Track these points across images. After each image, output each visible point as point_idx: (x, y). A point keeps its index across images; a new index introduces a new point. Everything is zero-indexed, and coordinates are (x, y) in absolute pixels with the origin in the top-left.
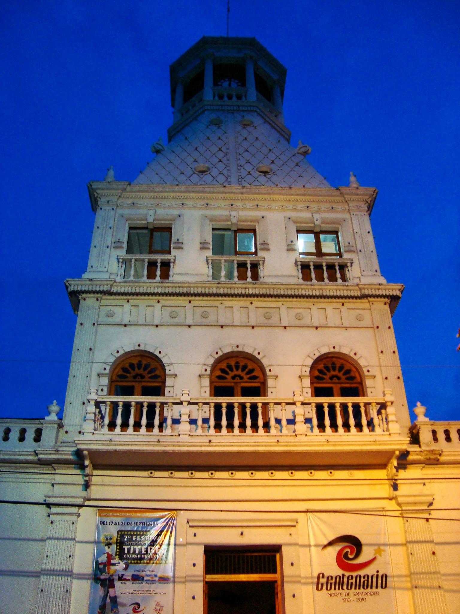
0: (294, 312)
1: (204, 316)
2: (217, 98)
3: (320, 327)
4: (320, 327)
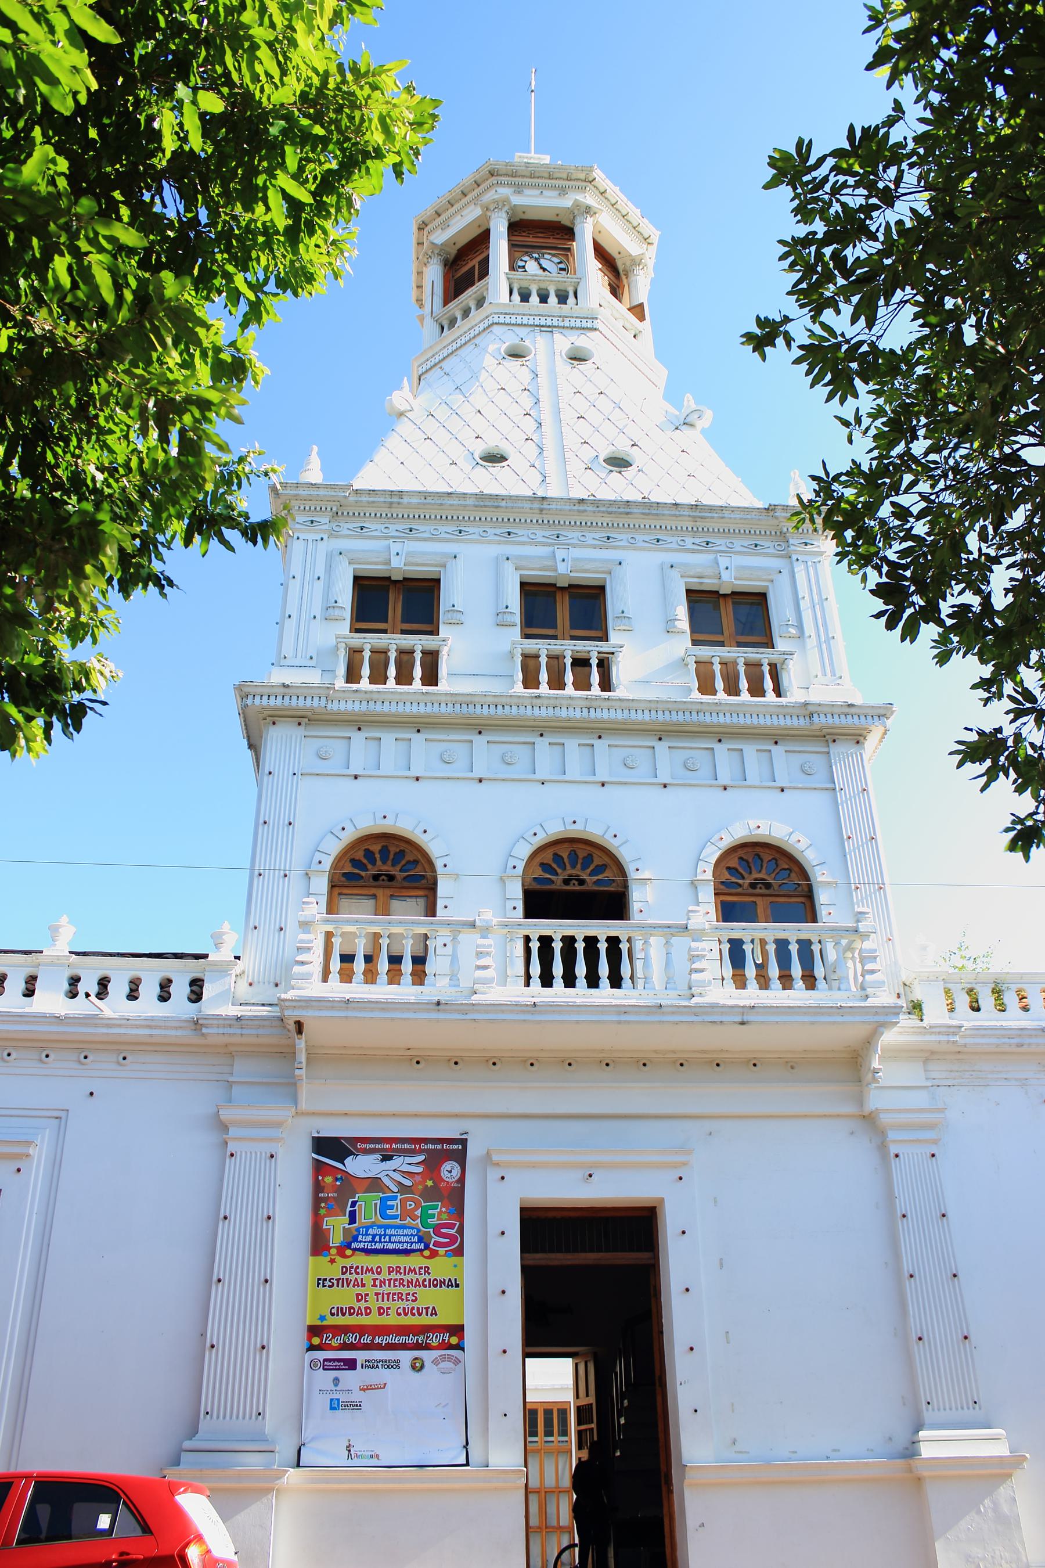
0: (680, 756)
1: (629, 762)
2: (516, 297)
3: (790, 788)
4: (790, 788)
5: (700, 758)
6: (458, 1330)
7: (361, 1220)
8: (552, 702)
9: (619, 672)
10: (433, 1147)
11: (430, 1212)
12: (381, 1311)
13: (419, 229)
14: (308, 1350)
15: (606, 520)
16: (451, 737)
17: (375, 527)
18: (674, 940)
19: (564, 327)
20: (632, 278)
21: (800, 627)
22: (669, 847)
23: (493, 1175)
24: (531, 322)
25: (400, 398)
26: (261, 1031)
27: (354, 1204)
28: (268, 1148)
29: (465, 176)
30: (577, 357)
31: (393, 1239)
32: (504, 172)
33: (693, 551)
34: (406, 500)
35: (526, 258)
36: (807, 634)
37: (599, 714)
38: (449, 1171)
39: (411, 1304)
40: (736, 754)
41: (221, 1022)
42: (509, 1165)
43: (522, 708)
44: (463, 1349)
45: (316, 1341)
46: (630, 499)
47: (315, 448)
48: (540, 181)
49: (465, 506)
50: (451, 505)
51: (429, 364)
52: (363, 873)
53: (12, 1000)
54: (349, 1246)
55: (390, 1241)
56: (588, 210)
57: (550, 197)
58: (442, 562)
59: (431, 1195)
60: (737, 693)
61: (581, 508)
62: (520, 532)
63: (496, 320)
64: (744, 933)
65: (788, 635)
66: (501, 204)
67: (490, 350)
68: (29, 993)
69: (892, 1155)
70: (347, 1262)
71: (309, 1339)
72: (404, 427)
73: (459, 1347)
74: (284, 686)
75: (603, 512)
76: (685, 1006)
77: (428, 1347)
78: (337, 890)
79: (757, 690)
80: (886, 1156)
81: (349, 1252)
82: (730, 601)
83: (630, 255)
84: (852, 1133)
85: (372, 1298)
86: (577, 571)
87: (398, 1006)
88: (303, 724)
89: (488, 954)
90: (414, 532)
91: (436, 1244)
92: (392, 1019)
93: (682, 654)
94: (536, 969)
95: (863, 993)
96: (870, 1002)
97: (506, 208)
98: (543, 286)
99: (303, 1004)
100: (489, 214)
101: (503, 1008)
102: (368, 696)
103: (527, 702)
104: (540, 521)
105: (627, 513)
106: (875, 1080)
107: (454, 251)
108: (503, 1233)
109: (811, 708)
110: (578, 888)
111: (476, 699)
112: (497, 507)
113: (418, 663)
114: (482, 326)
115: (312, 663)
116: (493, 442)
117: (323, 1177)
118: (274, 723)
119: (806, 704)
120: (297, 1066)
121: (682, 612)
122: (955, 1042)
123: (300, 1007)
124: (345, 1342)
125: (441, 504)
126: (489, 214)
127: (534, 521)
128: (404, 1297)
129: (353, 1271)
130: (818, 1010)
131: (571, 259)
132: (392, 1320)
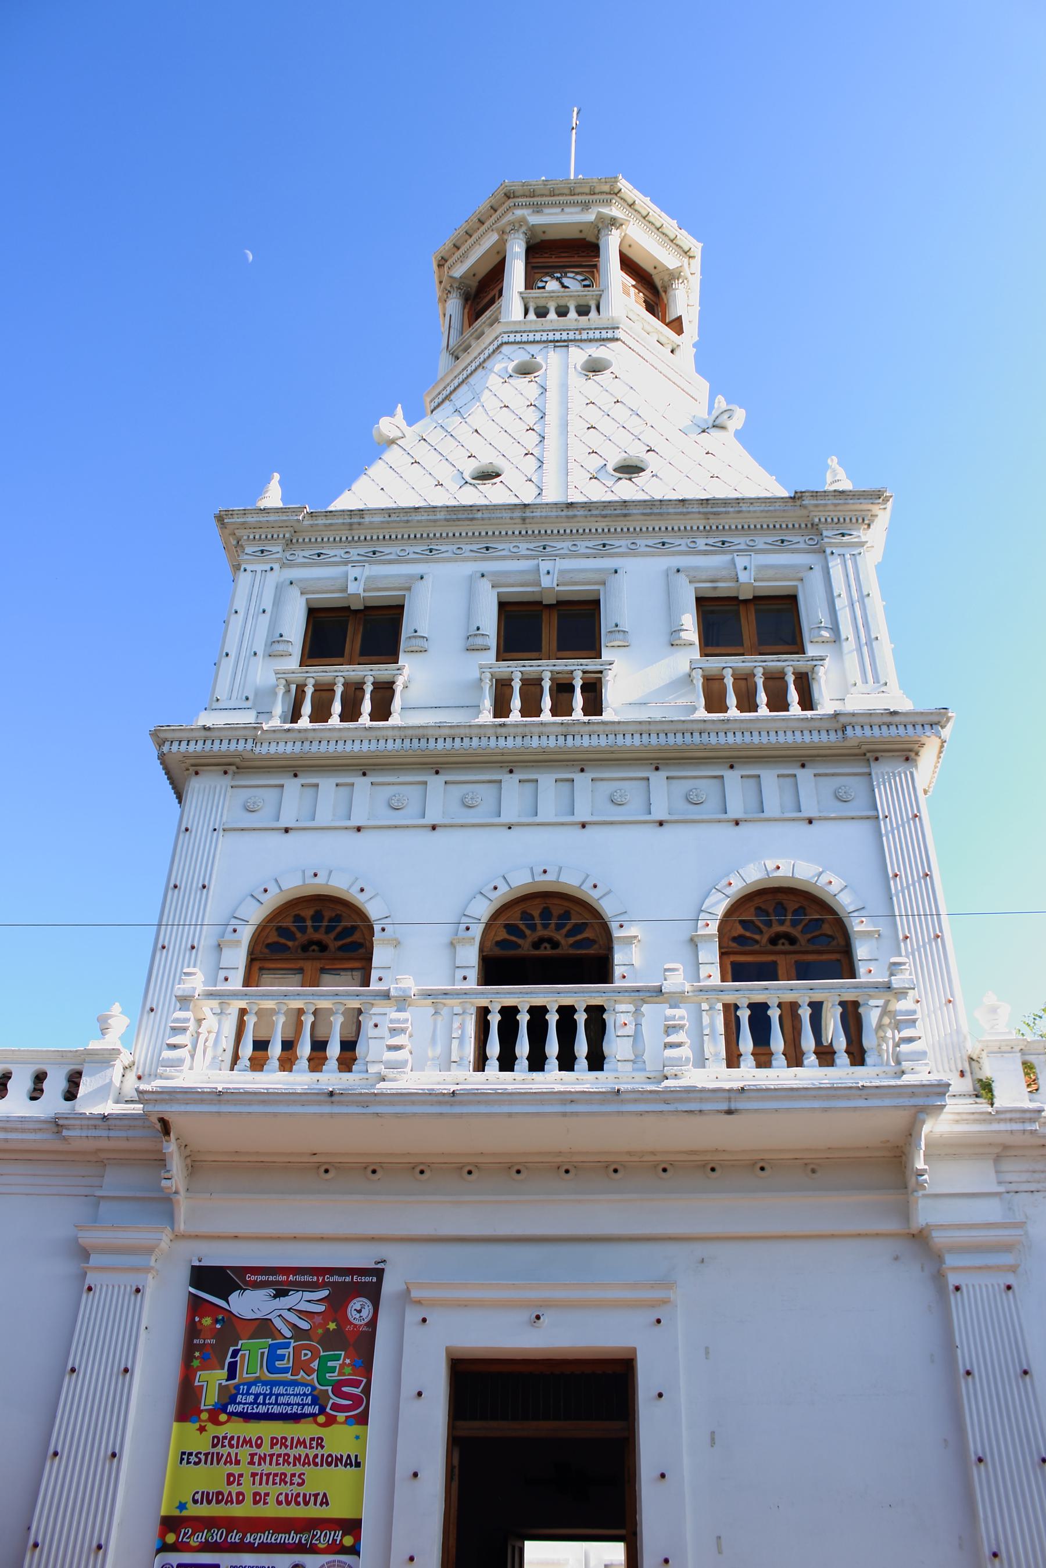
0: (681, 787)
1: (695, 800)
2: (532, 316)
3: (820, 819)
4: (820, 819)
5: (706, 788)
6: (353, 1526)
7: (243, 1375)
8: (520, 730)
9: (612, 695)
10: (341, 1279)
11: (330, 1364)
12: (258, 1498)
13: (440, 266)
14: (159, 1551)
15: (601, 525)
16: (402, 779)
17: (335, 553)
18: (645, 1008)
19: (581, 340)
20: (671, 293)
21: (835, 629)
22: (664, 894)
23: (412, 1316)
24: (544, 338)
25: (389, 426)
26: (130, 1133)
27: (235, 1353)
28: (133, 1280)
29: (482, 204)
30: (594, 368)
31: (281, 1400)
32: (521, 193)
33: (705, 553)
34: (367, 519)
35: (547, 279)
36: (843, 637)
37: (578, 741)
38: (358, 1310)
39: (296, 1489)
40: (752, 782)
41: (85, 1122)
42: (434, 1303)
43: (484, 740)
44: (358, 1554)
45: (171, 1538)
46: (627, 498)
47: (277, 476)
48: (561, 198)
49: (435, 521)
50: (418, 521)
51: (441, 397)
52: (290, 944)
53: (15, 1104)
54: (224, 1410)
55: (276, 1403)
56: (614, 222)
57: (571, 213)
58: (407, 585)
59: (331, 1341)
60: (754, 708)
61: (570, 513)
62: (500, 546)
63: (505, 339)
64: (738, 995)
65: (820, 639)
66: (517, 225)
67: (495, 370)
68: (70, 1095)
69: (951, 1288)
70: (221, 1431)
71: (162, 1536)
72: (393, 455)
73: (354, 1550)
74: (205, 728)
75: (596, 516)
76: (651, 1092)
77: (313, 1550)
78: (257, 965)
79: (778, 703)
80: (943, 1290)
81: (223, 1417)
82: (752, 609)
83: (668, 269)
84: (896, 1258)
85: (246, 1480)
86: (564, 585)
87: (281, 1098)
88: (230, 772)
89: (403, 1031)
90: (378, 554)
91: (336, 1407)
92: (275, 1115)
93: (687, 669)
94: (494, 1048)
95: (897, 1069)
96: (907, 1079)
97: (524, 229)
98: (562, 302)
99: (167, 1097)
100: (505, 237)
101: (414, 1098)
102: (302, 735)
103: (490, 732)
104: (524, 532)
105: (625, 515)
106: (921, 1186)
107: (474, 283)
108: (420, 1394)
109: (843, 720)
110: (549, 952)
111: (430, 732)
112: (472, 519)
113: (368, 696)
114: (491, 348)
115: (249, 704)
116: (487, 458)
117: (201, 1318)
118: (197, 773)
119: (836, 715)
120: (164, 1175)
121: (689, 624)
122: (1033, 1132)
123: (163, 1101)
124: (207, 1540)
125: (408, 521)
126: (505, 237)
127: (517, 533)
128: (288, 1479)
129: (226, 1442)
130: (833, 1092)
131: (596, 275)
132: (270, 1510)
